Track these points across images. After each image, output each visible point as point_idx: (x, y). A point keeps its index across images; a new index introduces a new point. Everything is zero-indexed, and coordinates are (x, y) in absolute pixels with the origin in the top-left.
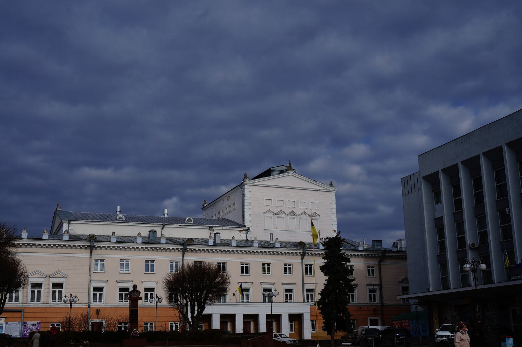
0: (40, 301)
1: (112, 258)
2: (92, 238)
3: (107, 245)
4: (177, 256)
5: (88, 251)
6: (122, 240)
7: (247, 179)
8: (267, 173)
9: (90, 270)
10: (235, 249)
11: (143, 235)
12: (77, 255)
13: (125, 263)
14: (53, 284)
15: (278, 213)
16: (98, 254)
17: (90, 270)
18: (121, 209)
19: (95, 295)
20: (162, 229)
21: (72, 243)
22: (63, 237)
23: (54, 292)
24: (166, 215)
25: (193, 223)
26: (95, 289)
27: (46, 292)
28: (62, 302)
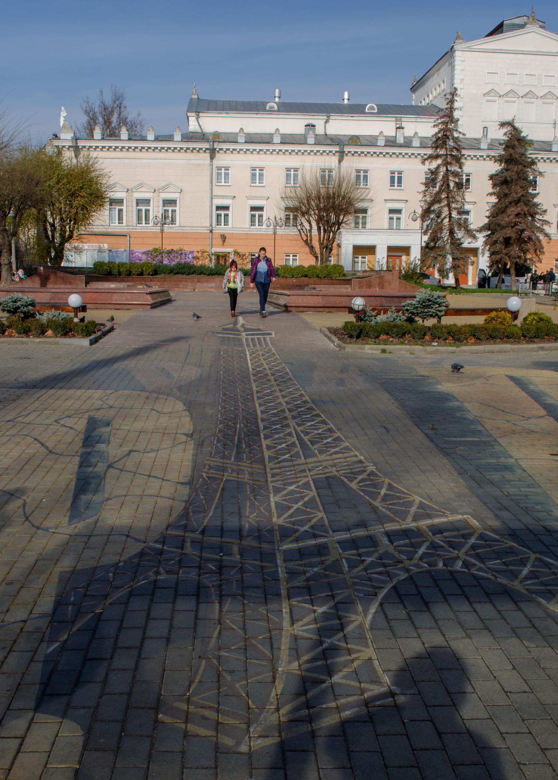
0: (227, 225)
1: (238, 163)
2: (217, 137)
3: (231, 146)
4: (332, 162)
5: (207, 155)
6: (251, 139)
7: (460, 41)
8: (498, 29)
9: (212, 183)
10: (153, 145)
11: (386, 133)
12: (193, 162)
13: (223, 171)
14: (163, 200)
15: (506, 94)
16: (221, 160)
17: (212, 183)
18: (280, 92)
19: (219, 216)
20: (326, 122)
21: (185, 145)
22: (173, 138)
23: (139, 211)
24: (346, 102)
25: (378, 113)
26: (218, 208)
27: (129, 211)
28: (151, 224)
